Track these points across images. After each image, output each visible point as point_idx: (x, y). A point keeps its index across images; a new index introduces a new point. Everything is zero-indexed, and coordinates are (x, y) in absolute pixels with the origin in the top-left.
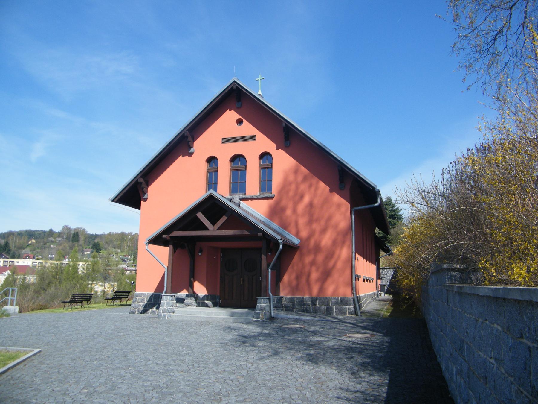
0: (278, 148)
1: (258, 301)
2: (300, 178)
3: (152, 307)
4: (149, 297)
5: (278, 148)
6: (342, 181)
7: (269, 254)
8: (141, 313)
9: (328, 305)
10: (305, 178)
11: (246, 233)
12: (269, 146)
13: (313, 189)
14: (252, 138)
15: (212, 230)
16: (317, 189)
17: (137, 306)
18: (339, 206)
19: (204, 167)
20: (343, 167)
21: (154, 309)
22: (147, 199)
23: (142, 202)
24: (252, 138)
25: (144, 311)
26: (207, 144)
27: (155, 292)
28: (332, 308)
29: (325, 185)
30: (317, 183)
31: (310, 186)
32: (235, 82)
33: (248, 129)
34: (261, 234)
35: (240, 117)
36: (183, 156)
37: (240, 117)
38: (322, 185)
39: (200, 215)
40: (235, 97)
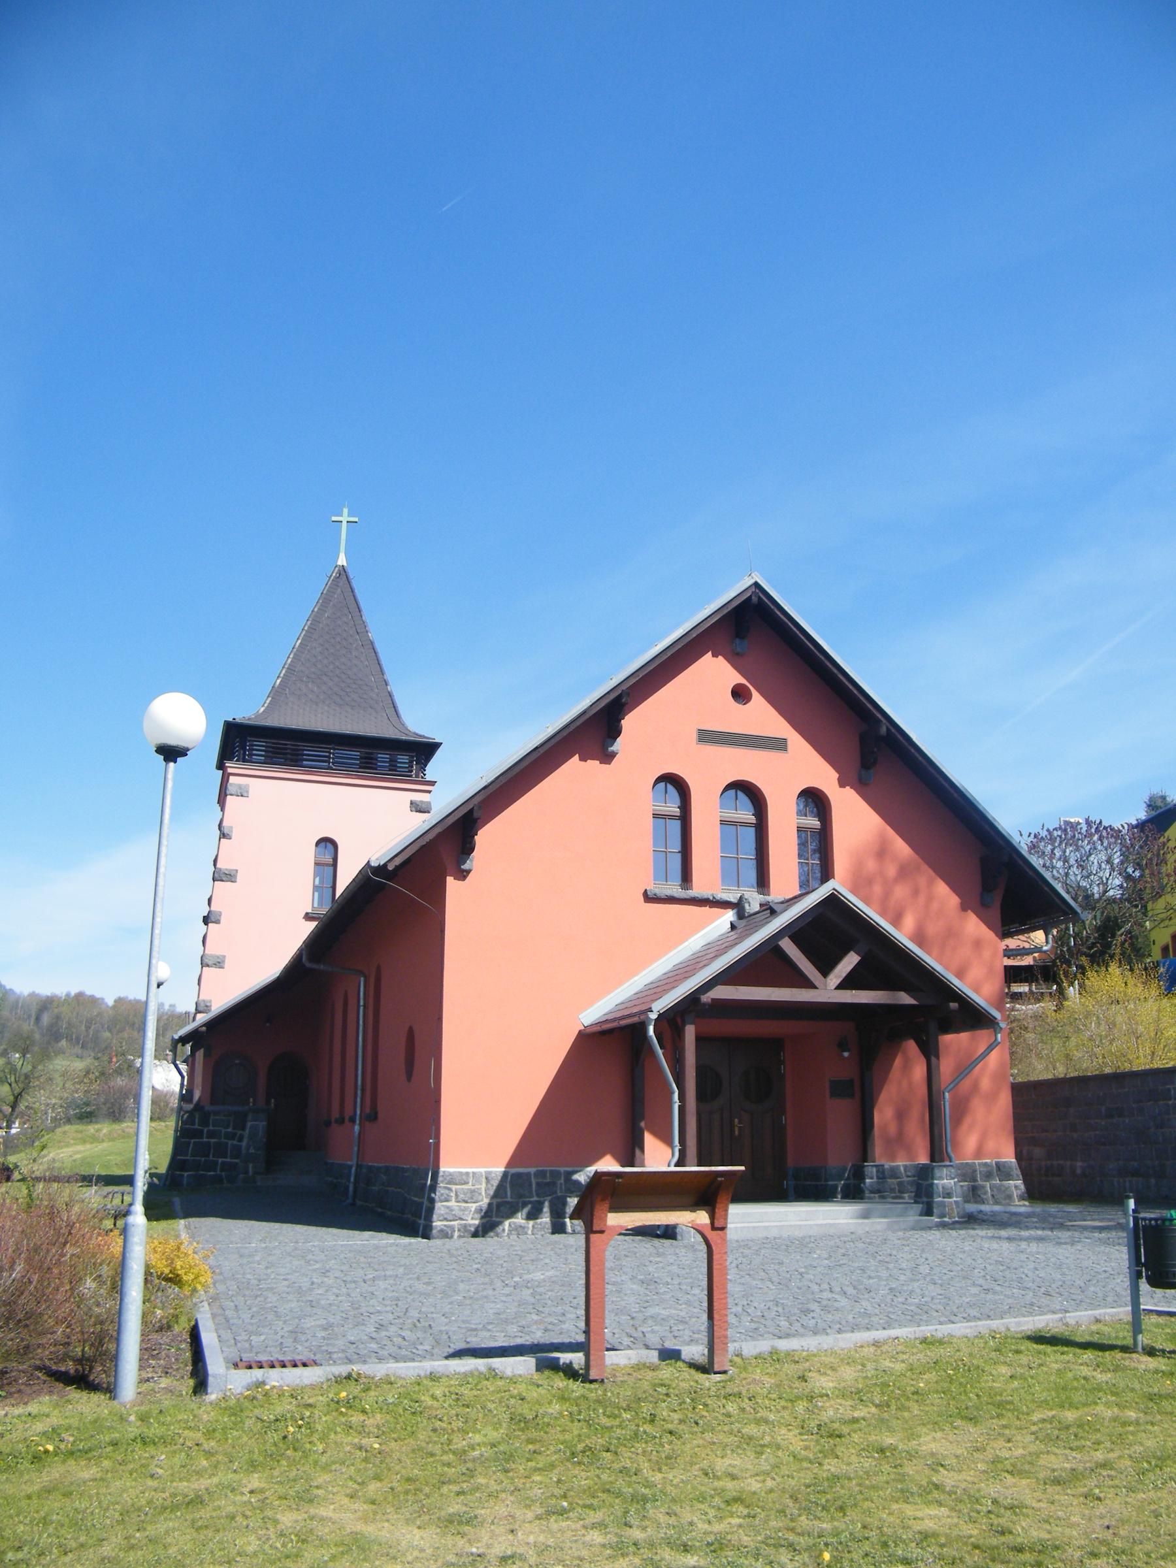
0: (842, 784)
1: (937, 1173)
2: (891, 871)
3: (512, 1213)
4: (495, 1183)
5: (842, 784)
6: (987, 886)
7: (846, 1054)
8: (475, 1235)
9: (975, 1180)
10: (904, 872)
11: (905, 999)
12: (825, 777)
13: (922, 899)
14: (779, 745)
15: (828, 989)
16: (930, 899)
17: (457, 1212)
18: (978, 944)
19: (646, 802)
20: (1015, 856)
21: (519, 1219)
22: (468, 872)
23: (450, 880)
24: (779, 745)
25: (487, 1226)
26: (655, 734)
27: (510, 1164)
28: (984, 1187)
29: (947, 889)
30: (930, 883)
31: (916, 892)
32: (756, 584)
33: (760, 715)
34: (956, 1005)
35: (744, 681)
36: (583, 759)
37: (744, 681)
38: (942, 889)
39: (787, 945)
40: (755, 631)
